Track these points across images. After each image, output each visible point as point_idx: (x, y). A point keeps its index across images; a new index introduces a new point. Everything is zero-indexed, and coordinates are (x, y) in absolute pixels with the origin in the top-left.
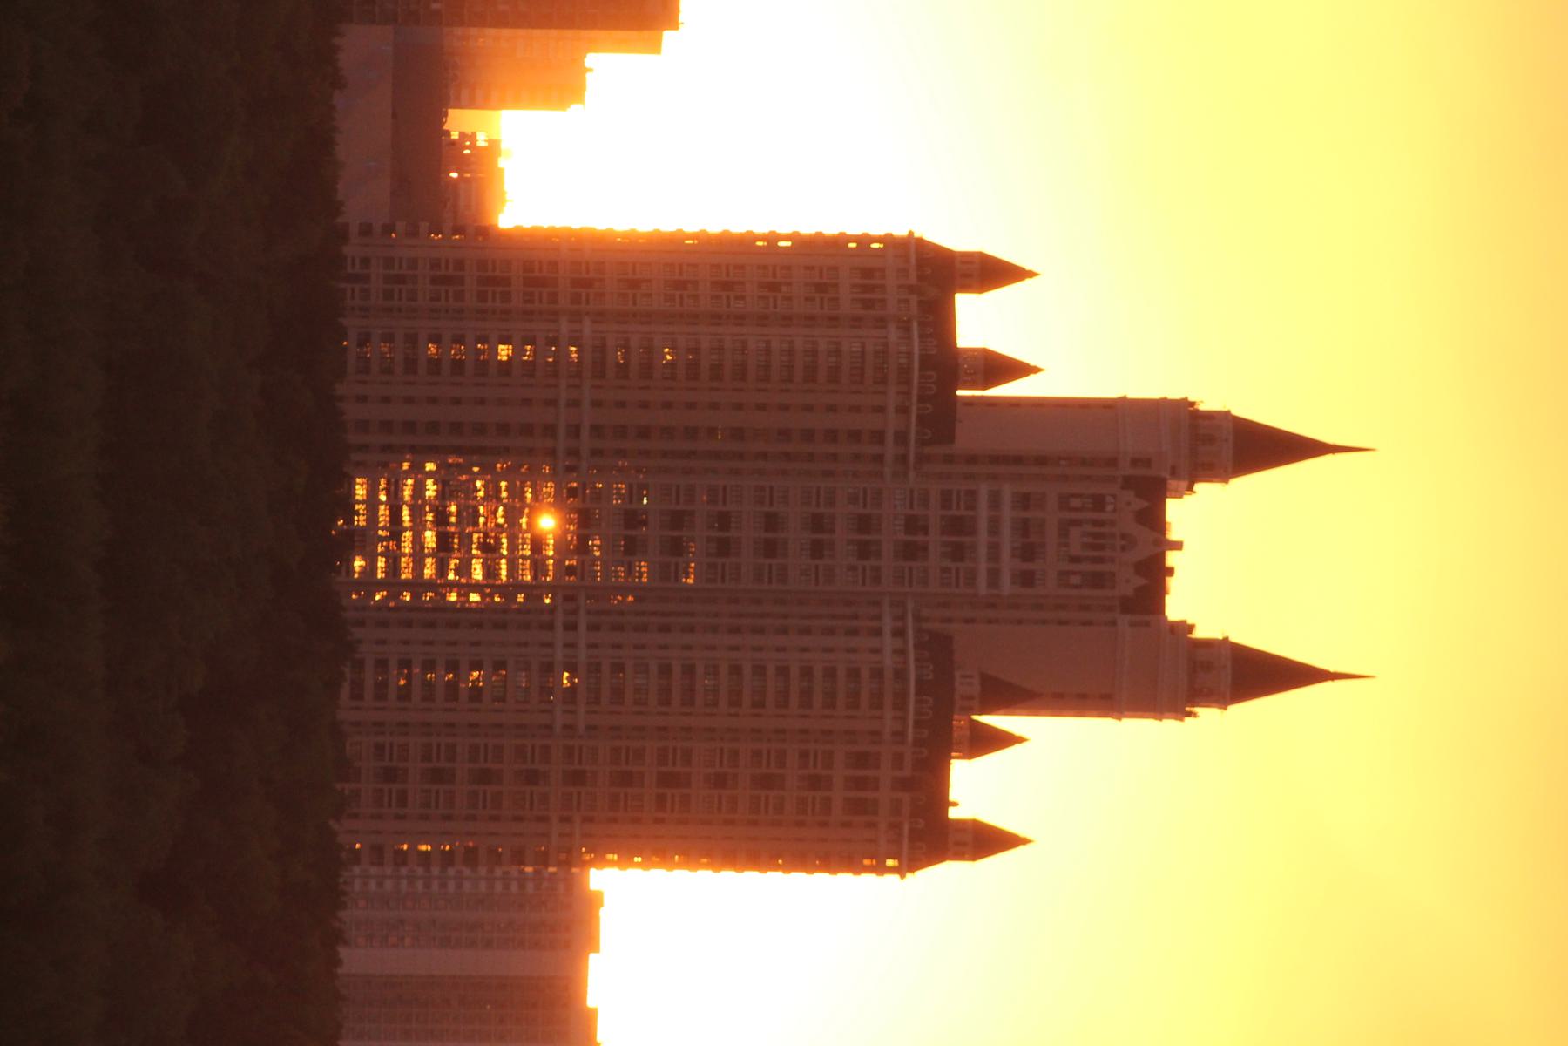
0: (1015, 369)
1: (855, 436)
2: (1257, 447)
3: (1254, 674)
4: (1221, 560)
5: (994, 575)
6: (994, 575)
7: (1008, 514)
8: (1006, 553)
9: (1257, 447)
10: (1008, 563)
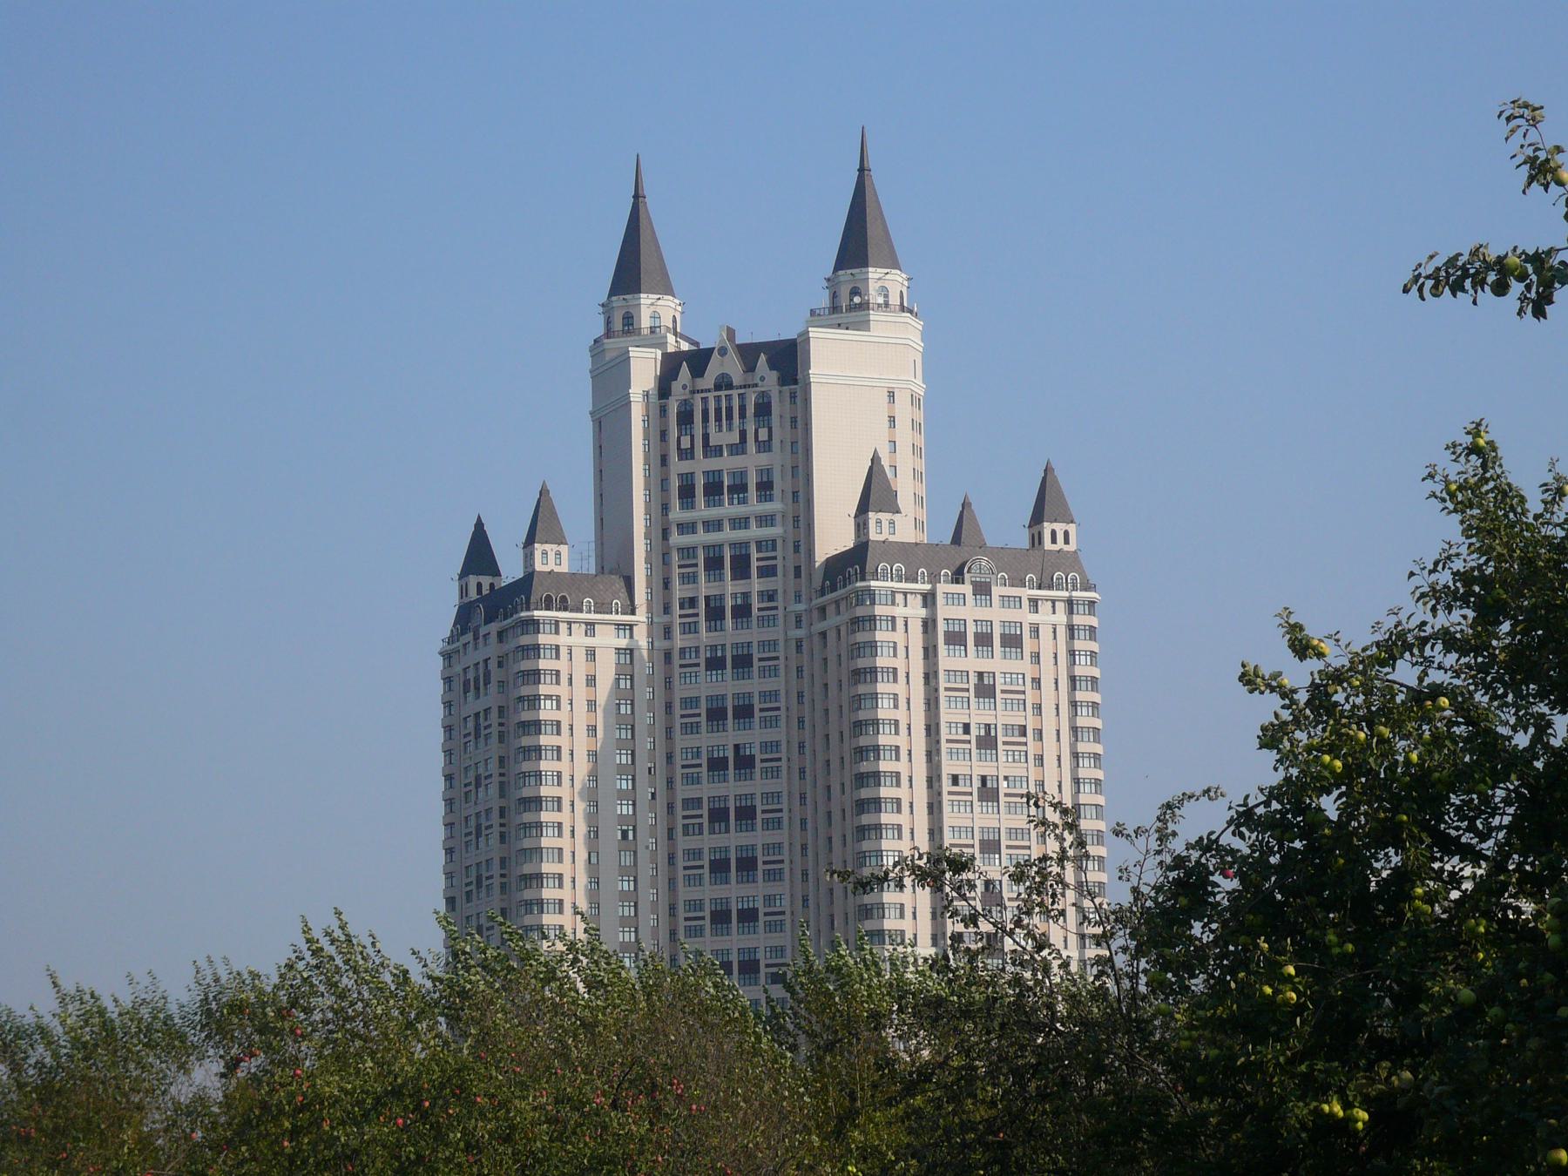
5: (766, 520)
6: (766, 520)
8: (738, 510)
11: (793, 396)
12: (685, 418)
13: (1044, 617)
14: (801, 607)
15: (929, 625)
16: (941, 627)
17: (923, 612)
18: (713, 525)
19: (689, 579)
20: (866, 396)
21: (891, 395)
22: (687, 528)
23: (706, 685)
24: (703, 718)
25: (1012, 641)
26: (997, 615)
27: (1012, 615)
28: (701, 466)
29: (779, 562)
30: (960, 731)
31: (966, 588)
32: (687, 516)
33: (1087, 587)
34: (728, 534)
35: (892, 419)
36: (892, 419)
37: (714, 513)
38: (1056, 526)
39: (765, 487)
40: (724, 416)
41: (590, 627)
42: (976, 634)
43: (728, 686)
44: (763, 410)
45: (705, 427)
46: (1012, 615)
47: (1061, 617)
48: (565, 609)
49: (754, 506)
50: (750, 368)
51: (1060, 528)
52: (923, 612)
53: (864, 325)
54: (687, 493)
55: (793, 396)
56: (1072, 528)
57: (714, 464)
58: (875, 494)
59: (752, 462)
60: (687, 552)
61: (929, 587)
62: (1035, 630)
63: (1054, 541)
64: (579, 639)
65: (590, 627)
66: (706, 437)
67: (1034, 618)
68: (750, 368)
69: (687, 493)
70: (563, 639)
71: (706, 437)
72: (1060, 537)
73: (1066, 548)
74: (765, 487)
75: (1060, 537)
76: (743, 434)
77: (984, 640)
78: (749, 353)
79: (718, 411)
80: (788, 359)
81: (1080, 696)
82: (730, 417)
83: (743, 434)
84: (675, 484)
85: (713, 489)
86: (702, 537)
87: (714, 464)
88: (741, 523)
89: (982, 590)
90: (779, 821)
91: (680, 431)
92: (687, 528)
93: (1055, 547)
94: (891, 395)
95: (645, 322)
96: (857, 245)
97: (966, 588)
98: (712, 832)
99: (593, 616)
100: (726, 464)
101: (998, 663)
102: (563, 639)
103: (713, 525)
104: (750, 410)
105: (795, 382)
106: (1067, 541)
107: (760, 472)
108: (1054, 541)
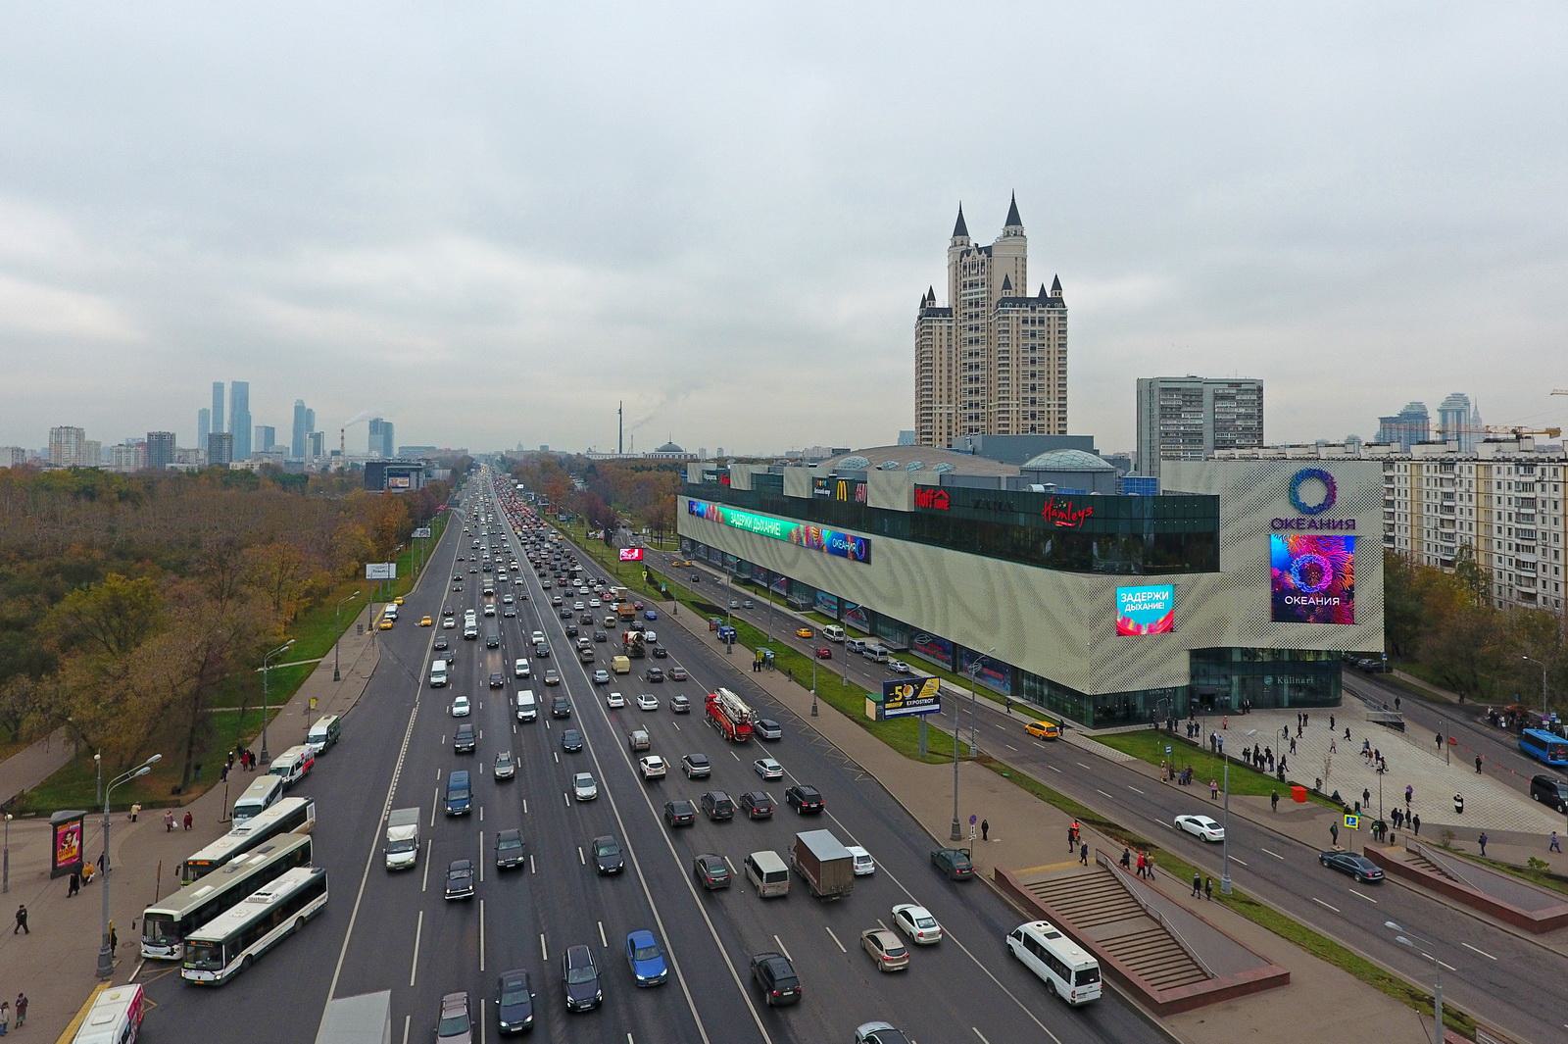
1: (949, 421)
2: (961, 228)
3: (1013, 217)
4: (985, 231)
5: (983, 292)
7: (968, 291)
9: (961, 228)
10: (980, 289)
12: (965, 267)
25: (1041, 322)
43: (973, 335)
46: (1041, 315)
62: (1049, 318)
65: (1049, 312)
74: (983, 284)
78: (980, 251)
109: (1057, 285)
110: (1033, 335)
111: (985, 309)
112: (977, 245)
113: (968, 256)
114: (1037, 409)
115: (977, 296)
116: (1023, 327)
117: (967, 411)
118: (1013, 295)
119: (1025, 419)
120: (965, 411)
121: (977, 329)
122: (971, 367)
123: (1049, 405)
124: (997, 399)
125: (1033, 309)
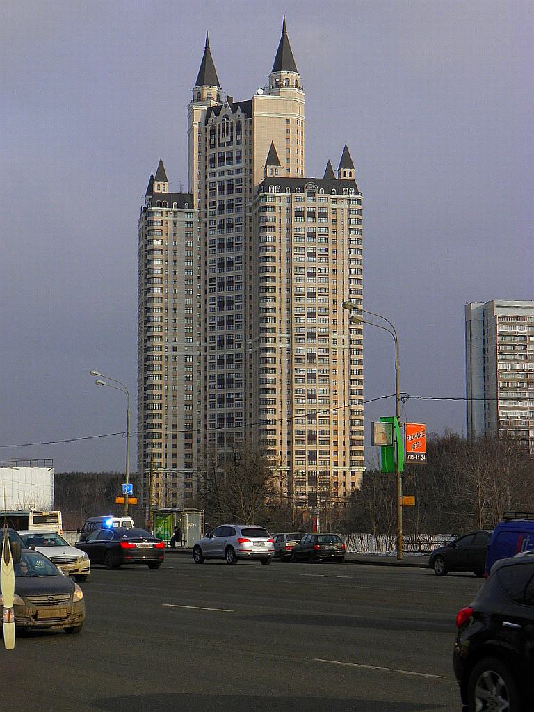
0: (152, 176)
5: (238, 171)
6: (238, 171)
7: (217, 168)
11: (250, 122)
12: (213, 132)
13: (339, 205)
14: (251, 204)
15: (289, 208)
16: (294, 210)
17: (287, 204)
18: (221, 173)
19: (214, 194)
20: (275, 120)
21: (288, 120)
22: (213, 175)
23: (217, 235)
24: (216, 248)
25: (323, 215)
26: (316, 205)
27: (323, 205)
28: (217, 150)
29: (243, 187)
30: (325, 251)
31: (305, 195)
32: (213, 170)
33: (357, 193)
34: (226, 177)
35: (288, 130)
36: (288, 130)
37: (222, 168)
38: (346, 170)
39: (239, 158)
40: (225, 131)
41: (334, 200)
42: (308, 212)
44: (239, 128)
45: (219, 136)
46: (323, 205)
47: (346, 206)
48: (166, 207)
49: (235, 166)
50: (234, 111)
51: (348, 171)
52: (287, 204)
53: (278, 94)
54: (213, 161)
55: (250, 122)
56: (352, 170)
57: (222, 149)
58: (273, 159)
59: (234, 148)
60: (212, 184)
61: (289, 194)
62: (334, 210)
63: (345, 176)
64: (170, 218)
65: (334, 200)
66: (219, 139)
67: (334, 206)
68: (234, 111)
69: (213, 161)
70: (164, 218)
71: (219, 139)
72: (348, 174)
73: (350, 178)
75: (348, 174)
76: (232, 137)
77: (311, 215)
78: (234, 107)
79: (224, 129)
80: (248, 107)
81: (352, 236)
82: (227, 132)
83: (232, 137)
84: (209, 158)
85: (221, 160)
86: (217, 178)
87: (222, 149)
88: (230, 172)
89: (311, 195)
90: (210, 282)
91: (237, 133)
92: (213, 175)
93: (345, 178)
94: (288, 120)
95: (205, 96)
96: (283, 60)
97: (305, 195)
98: (218, 291)
99: (177, 209)
100: (226, 149)
101: (317, 223)
102: (164, 218)
103: (221, 173)
104: (217, 132)
105: (251, 117)
106: (350, 176)
107: (237, 152)
108: (345, 176)
109: (346, 161)
110: (312, 235)
111: (242, 195)
112: (230, 99)
113: (217, 114)
114: (318, 447)
115: (230, 177)
116: (297, 221)
117: (216, 352)
118: (282, 174)
119: (299, 361)
120: (212, 353)
121: (230, 226)
122: (221, 285)
123: (335, 341)
124: (258, 391)
125: (311, 195)
